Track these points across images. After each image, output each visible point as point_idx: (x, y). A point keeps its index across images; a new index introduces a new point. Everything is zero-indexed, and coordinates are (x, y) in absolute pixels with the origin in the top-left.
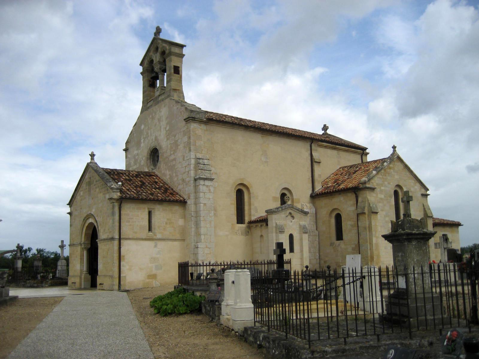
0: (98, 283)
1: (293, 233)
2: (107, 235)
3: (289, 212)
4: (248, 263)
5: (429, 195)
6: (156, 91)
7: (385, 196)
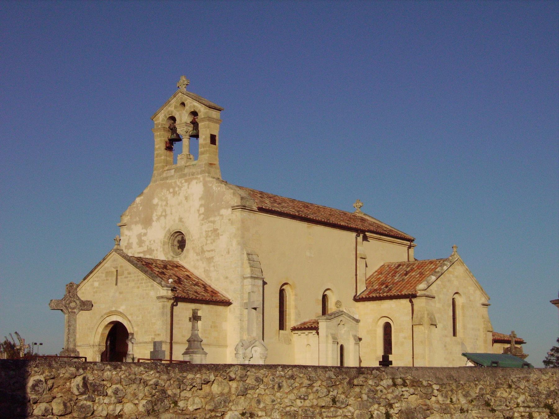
2: (152, 338)
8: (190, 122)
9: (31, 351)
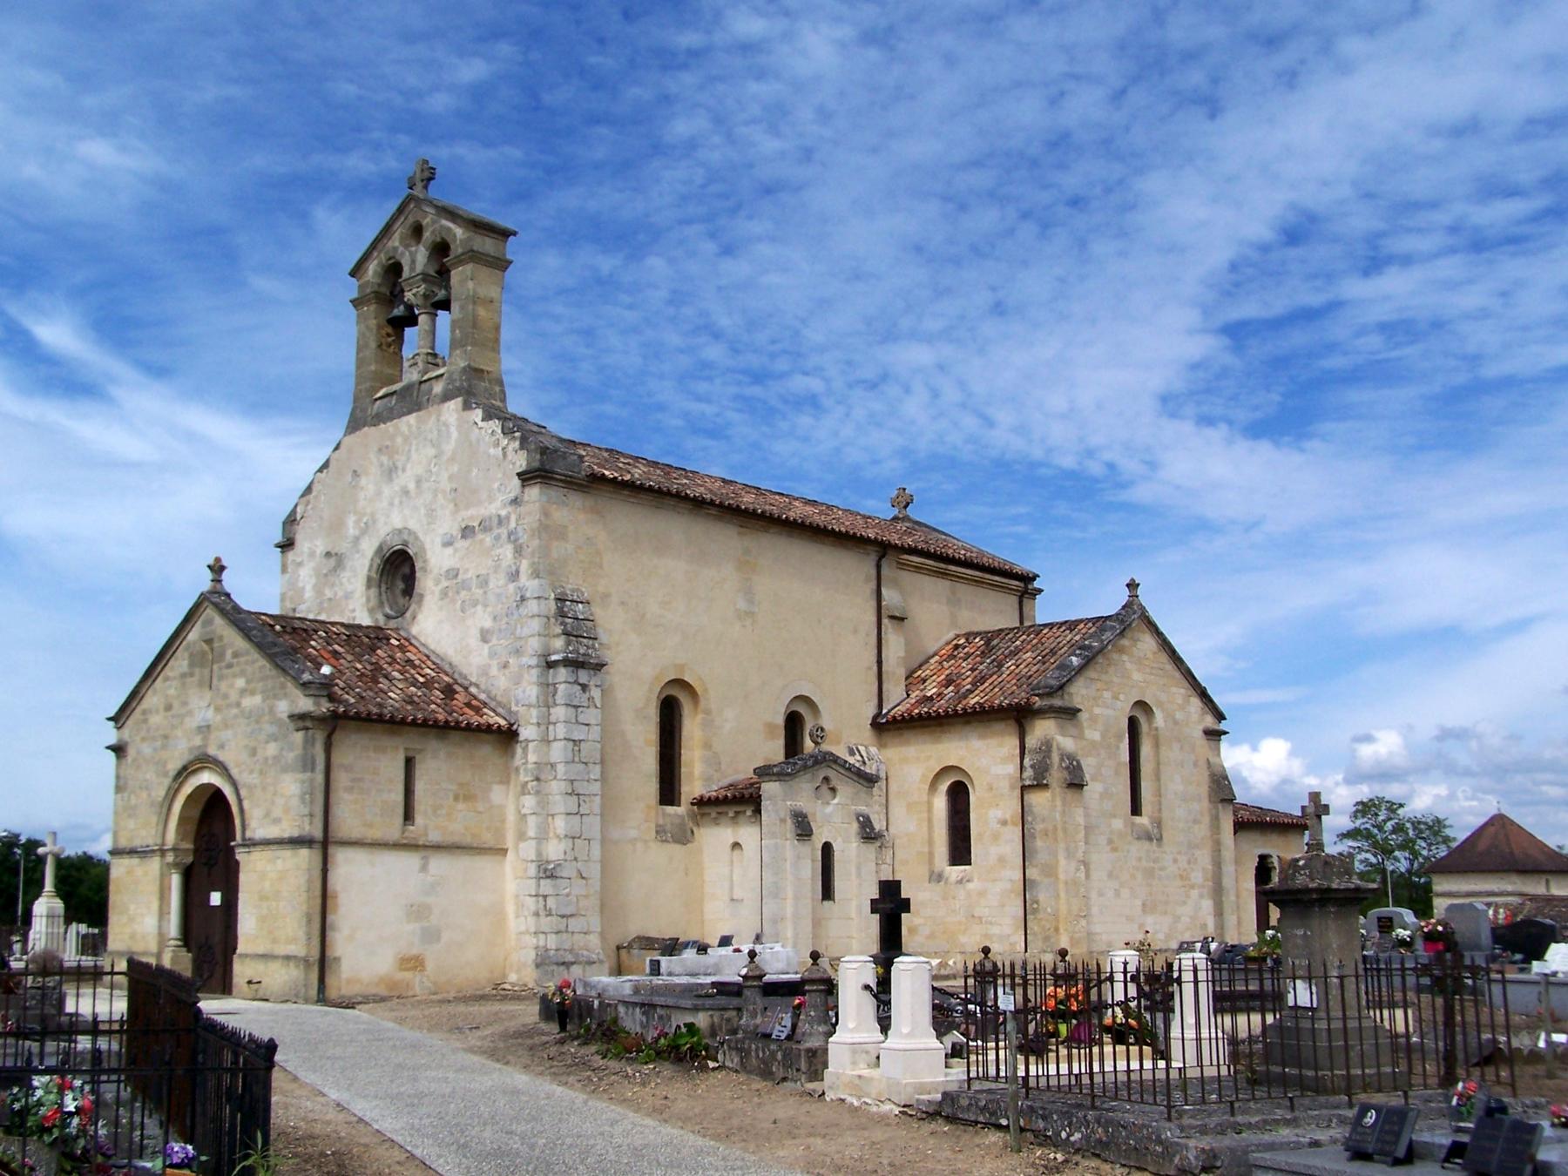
1: (832, 842)
5: (1225, 733)
7: (1103, 736)
9: (1058, 803)
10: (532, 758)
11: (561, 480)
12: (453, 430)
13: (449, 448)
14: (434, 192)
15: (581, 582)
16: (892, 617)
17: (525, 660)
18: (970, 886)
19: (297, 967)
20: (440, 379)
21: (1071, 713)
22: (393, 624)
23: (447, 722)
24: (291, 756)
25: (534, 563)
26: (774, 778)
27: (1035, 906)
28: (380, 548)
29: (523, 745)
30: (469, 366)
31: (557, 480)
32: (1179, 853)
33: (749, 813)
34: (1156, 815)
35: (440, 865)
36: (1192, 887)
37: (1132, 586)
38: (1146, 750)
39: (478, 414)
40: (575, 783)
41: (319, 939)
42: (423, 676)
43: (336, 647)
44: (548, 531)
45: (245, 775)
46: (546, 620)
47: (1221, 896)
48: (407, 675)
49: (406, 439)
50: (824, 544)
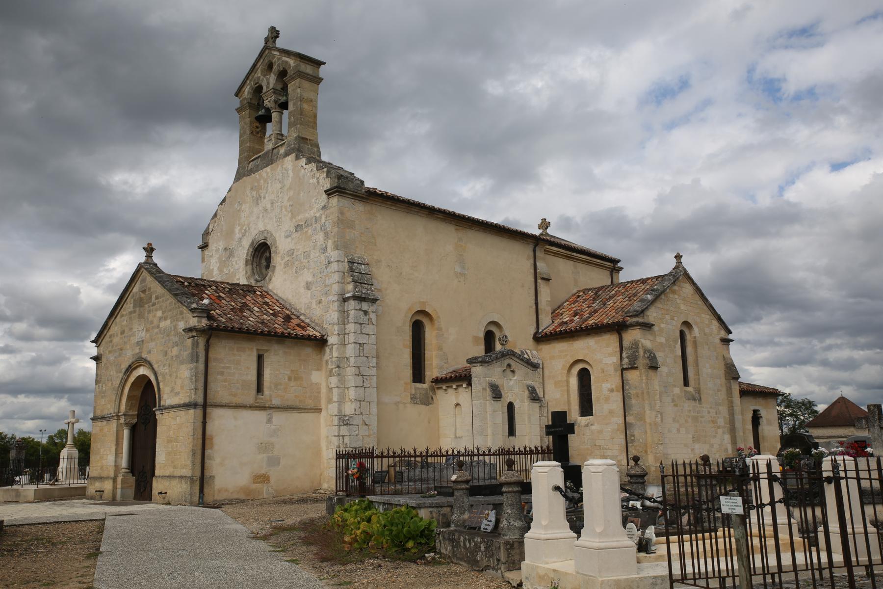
0: (155, 492)
1: (513, 402)
3: (507, 363)
4: (421, 453)
5: (732, 341)
6: (266, 141)
7: (667, 340)
8: (281, 89)
10: (335, 354)
11: (350, 194)
12: (290, 172)
13: (288, 182)
14: (279, 43)
15: (364, 253)
16: (543, 279)
17: (331, 298)
18: (593, 427)
19: (186, 483)
20: (283, 146)
21: (648, 326)
22: (259, 284)
23: (283, 333)
24: (186, 354)
25: (335, 242)
26: (479, 364)
27: (633, 438)
28: (252, 243)
29: (330, 347)
30: (298, 136)
31: (347, 193)
32: (711, 408)
33: (465, 385)
34: (697, 386)
35: (279, 418)
36: (719, 427)
37: (678, 257)
38: (689, 349)
39: (303, 161)
40: (361, 369)
41: (200, 466)
42: (273, 310)
43: (221, 294)
44: (343, 222)
45: (161, 368)
46: (342, 274)
47: (735, 433)
48: (263, 309)
49: (266, 181)
50: (504, 237)
